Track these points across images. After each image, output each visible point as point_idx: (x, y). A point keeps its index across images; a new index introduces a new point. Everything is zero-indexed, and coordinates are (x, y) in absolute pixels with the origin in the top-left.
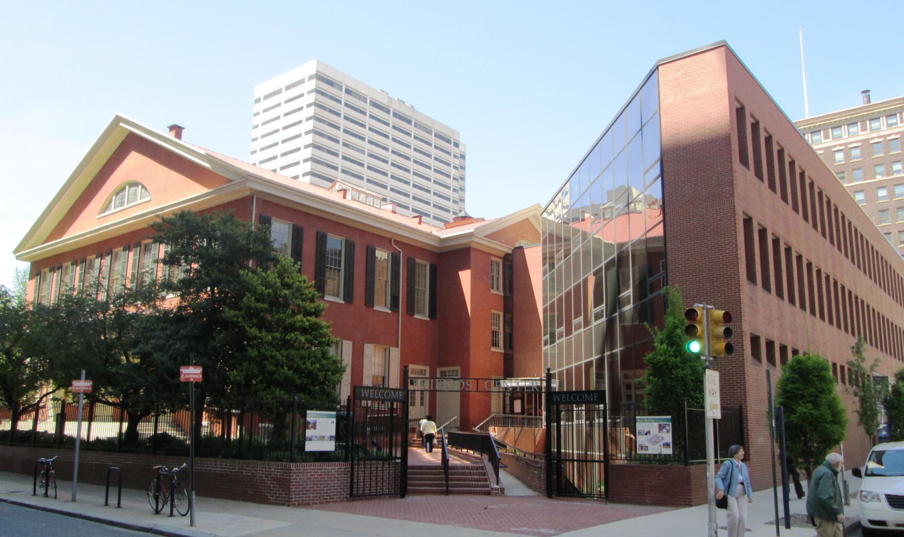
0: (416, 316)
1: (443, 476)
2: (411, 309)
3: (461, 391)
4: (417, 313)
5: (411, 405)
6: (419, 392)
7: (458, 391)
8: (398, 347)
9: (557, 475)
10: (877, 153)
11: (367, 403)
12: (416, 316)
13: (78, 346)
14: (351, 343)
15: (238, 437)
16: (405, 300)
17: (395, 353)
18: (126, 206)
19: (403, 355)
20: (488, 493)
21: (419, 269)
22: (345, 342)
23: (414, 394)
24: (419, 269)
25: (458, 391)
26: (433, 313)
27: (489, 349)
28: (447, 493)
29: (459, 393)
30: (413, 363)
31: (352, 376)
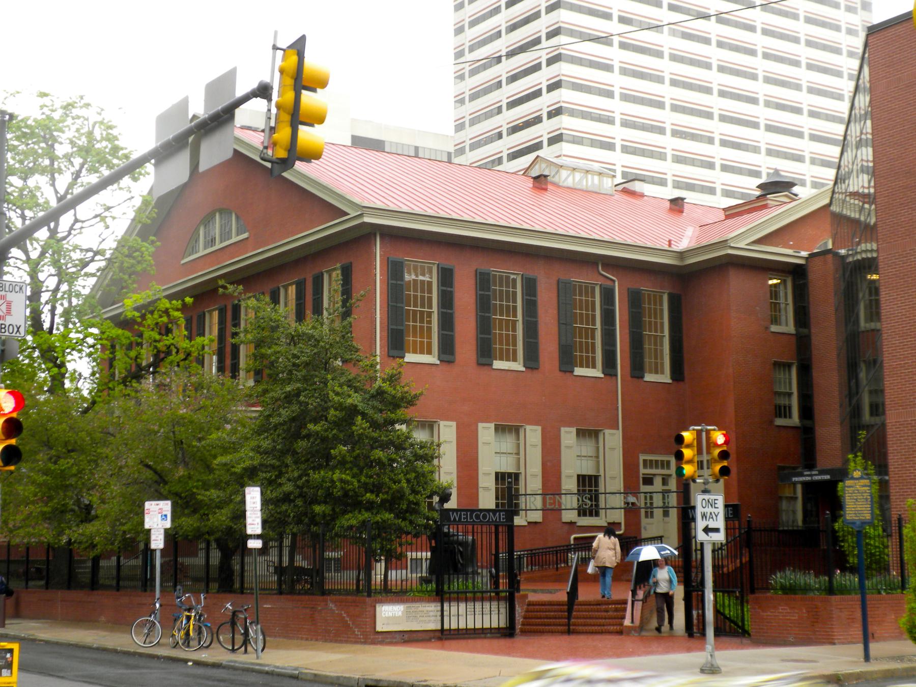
0: (649, 377)
1: (566, 614)
2: (637, 368)
3: (624, 508)
4: (650, 372)
5: (647, 516)
6: (660, 495)
7: (621, 508)
8: (618, 429)
9: (610, 604)
10: (240, 515)
11: (449, 529)
12: (649, 377)
13: (180, 431)
14: (539, 429)
15: (390, 572)
16: (627, 355)
17: (613, 439)
18: (218, 246)
19: (627, 439)
20: (620, 633)
21: (649, 303)
22: (529, 428)
23: (651, 498)
24: (649, 303)
25: (621, 508)
26: (678, 372)
27: (772, 422)
28: (569, 632)
29: (623, 510)
30: (645, 452)
31: (543, 477)
